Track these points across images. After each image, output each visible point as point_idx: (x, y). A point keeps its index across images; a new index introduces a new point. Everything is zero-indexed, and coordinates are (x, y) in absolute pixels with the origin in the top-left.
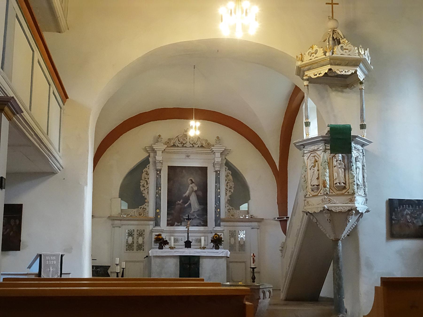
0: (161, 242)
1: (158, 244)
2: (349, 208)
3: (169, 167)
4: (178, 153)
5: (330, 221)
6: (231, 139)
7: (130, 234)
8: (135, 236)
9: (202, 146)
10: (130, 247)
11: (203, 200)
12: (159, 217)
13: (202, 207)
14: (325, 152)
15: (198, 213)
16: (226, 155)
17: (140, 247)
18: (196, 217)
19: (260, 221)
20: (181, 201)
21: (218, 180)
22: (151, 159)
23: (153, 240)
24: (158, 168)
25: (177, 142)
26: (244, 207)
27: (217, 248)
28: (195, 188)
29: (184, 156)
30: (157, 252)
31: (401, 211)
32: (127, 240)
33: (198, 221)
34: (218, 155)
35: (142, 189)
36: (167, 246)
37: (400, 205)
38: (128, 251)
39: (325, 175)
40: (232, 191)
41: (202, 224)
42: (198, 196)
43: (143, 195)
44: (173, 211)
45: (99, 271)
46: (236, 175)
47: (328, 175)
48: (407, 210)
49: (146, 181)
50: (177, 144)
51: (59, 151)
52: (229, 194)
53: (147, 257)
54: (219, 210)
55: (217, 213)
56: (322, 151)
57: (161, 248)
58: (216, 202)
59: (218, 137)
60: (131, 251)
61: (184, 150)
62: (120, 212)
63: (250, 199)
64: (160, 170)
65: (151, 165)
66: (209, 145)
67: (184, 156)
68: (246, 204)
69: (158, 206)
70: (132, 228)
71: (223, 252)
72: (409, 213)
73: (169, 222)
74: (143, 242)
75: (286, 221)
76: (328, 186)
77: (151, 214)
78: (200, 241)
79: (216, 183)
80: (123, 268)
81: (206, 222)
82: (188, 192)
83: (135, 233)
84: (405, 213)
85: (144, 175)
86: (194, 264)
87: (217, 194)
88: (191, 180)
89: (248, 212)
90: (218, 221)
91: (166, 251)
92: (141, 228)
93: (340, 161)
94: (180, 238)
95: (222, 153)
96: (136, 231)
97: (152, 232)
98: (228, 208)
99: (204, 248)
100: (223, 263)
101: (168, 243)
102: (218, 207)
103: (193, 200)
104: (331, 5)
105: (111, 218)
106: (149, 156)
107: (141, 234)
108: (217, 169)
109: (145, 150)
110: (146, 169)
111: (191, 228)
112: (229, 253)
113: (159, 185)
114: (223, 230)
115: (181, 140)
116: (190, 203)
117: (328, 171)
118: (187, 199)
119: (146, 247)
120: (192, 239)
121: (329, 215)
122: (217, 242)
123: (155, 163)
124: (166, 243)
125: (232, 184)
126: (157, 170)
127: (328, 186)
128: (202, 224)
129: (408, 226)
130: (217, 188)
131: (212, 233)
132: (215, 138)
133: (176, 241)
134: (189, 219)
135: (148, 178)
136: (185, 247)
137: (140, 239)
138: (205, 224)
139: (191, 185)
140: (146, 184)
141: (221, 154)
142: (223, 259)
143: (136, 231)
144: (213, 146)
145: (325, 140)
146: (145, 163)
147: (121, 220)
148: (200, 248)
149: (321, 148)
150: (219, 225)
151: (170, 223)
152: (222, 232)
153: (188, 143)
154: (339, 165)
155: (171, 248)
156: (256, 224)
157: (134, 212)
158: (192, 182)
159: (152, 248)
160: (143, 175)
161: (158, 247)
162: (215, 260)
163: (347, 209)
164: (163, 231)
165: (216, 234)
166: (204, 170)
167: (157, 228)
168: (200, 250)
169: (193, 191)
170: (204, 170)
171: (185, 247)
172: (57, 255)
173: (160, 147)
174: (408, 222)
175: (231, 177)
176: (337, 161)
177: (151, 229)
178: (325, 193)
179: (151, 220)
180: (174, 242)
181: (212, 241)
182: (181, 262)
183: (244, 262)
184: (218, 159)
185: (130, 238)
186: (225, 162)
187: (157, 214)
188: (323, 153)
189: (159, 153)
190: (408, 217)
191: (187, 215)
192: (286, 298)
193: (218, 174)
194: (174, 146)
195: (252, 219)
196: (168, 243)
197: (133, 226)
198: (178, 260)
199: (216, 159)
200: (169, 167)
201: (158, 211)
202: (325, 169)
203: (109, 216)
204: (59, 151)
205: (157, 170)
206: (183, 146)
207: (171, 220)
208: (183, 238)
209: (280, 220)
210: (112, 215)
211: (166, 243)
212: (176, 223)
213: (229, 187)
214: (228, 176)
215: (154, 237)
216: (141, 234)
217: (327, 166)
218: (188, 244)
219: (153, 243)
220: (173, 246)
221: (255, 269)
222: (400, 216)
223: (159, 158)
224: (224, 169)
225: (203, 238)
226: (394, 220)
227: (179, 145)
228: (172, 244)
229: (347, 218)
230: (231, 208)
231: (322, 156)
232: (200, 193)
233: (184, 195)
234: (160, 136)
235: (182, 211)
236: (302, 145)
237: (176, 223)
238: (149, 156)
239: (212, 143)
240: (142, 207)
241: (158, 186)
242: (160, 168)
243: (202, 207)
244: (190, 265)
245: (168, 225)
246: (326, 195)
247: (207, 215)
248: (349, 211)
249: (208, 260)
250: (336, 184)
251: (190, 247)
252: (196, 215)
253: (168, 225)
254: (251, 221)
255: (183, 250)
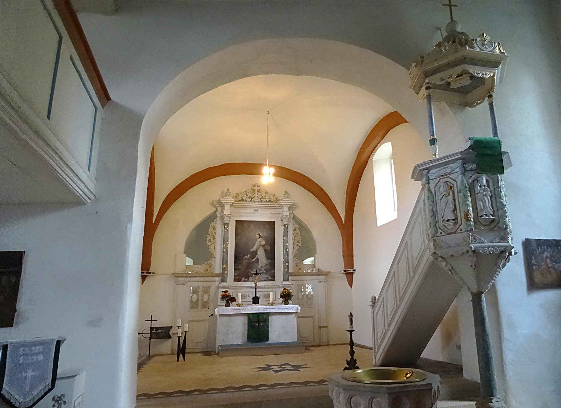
0: (229, 300)
1: (225, 301)
2: (503, 249)
3: (237, 222)
4: (246, 207)
5: (476, 267)
6: (299, 194)
7: (195, 291)
8: (200, 293)
9: (270, 201)
10: (194, 305)
11: (271, 254)
12: (226, 272)
13: (270, 261)
14: (464, 175)
15: (266, 267)
16: (293, 210)
17: (205, 305)
18: (263, 272)
19: (326, 274)
20: (249, 256)
21: (286, 234)
22: (218, 214)
23: (220, 297)
24: (226, 222)
25: (246, 196)
26: (308, 261)
27: (286, 303)
28: (263, 243)
29: (252, 211)
30: (223, 310)
31: (540, 254)
32: (192, 297)
33: (266, 276)
34: (286, 209)
35: (209, 244)
36: (234, 303)
37: (538, 246)
38: (192, 310)
39: (468, 205)
40: (300, 244)
41: (270, 278)
42: (266, 251)
43: (210, 250)
44: (240, 267)
45: (250, 226)
46: (302, 229)
47: (470, 204)
48: (546, 253)
49: (213, 236)
50: (245, 198)
51: (89, 170)
52: (297, 248)
53: (212, 315)
54: (287, 264)
55: (286, 267)
56: (459, 173)
57: (228, 305)
58: (284, 256)
59: (286, 192)
60: (196, 310)
61: (252, 204)
62: (185, 268)
63: (316, 253)
64: (228, 224)
65: (218, 219)
66: (277, 200)
67: (252, 211)
68: (313, 258)
69: (225, 261)
70: (197, 285)
71: (292, 308)
72: (549, 256)
73: (236, 278)
74: (209, 299)
75: (352, 273)
76: (472, 220)
77: (218, 269)
78: (268, 296)
79: (284, 236)
80: (186, 331)
81: (274, 277)
82: (256, 246)
83: (201, 290)
84: (544, 256)
85: (211, 230)
86: (263, 322)
87: (286, 248)
88: (259, 234)
89: (313, 266)
90: (287, 275)
91: (233, 309)
92: (206, 284)
93: (484, 186)
94: (247, 294)
95: (290, 207)
96: (201, 288)
97: (218, 288)
98: (295, 262)
99: (272, 304)
100: (293, 318)
101: (235, 300)
102: (286, 261)
103: (261, 254)
104: (452, 3)
105: (176, 275)
106: (216, 211)
107: (206, 291)
108: (285, 223)
109: (213, 205)
110: (213, 224)
111: (260, 284)
112: (300, 308)
113: (226, 240)
114: (291, 285)
115: (249, 194)
116: (258, 259)
117: (470, 199)
118: (255, 253)
119: (211, 305)
120: (260, 295)
121: (475, 259)
122: (286, 297)
123: (222, 217)
124: (233, 300)
125: (299, 238)
126: (225, 225)
127: (472, 220)
128: (270, 278)
129: (550, 273)
130: (286, 242)
131: (279, 288)
132: (284, 193)
133: (243, 297)
134: (256, 274)
135: (215, 233)
136: (253, 303)
137: (206, 296)
138: (273, 279)
139: (258, 240)
140: (212, 239)
141: (290, 208)
142: (294, 315)
143: (201, 288)
144: (281, 200)
145: (464, 159)
146: (212, 218)
147: (186, 277)
148: (269, 304)
149: (458, 170)
150: (288, 280)
151: (237, 279)
152: (290, 286)
153: (256, 198)
154: (484, 191)
155: (239, 305)
156: (323, 277)
157: (201, 268)
158: (260, 237)
159: (218, 306)
160: (210, 230)
161: (225, 304)
162: (284, 316)
163: (498, 250)
164: (229, 287)
165: (285, 289)
166: (272, 224)
167: (224, 284)
168: (268, 307)
169: (261, 245)
170: (272, 224)
171: (253, 303)
172: (45, 344)
173: (228, 200)
174: (549, 267)
175: (298, 231)
176: (480, 186)
177: (217, 285)
178: (469, 229)
179: (217, 276)
180: (242, 299)
181: (281, 297)
182: (249, 319)
183: (312, 317)
184: (286, 212)
185: (195, 296)
186: (292, 217)
187: (224, 270)
188: (460, 176)
189: (227, 207)
190: (548, 260)
191: (255, 270)
192: (383, 363)
193: (286, 227)
194: (242, 200)
195: (319, 273)
196: (235, 300)
197: (199, 283)
198: (247, 318)
199: (284, 213)
200: (237, 222)
201: (225, 266)
202: (466, 197)
203: (173, 272)
204: (89, 170)
205: (225, 225)
206: (251, 200)
207: (237, 275)
208: (250, 294)
209: (346, 273)
210: (176, 272)
211: (233, 300)
212: (243, 279)
213: (296, 241)
214: (295, 230)
215: (220, 294)
216: (206, 291)
217: (469, 193)
218: (256, 300)
219: (219, 300)
220: (240, 303)
221: (353, 332)
222: (539, 260)
223: (227, 211)
224: (291, 224)
225: (271, 293)
226: (535, 265)
227: (247, 199)
228: (239, 300)
229: (497, 263)
230: (299, 261)
231: (459, 180)
232: (268, 248)
233: (252, 250)
234: (228, 190)
235: (249, 266)
236: (426, 169)
237: (243, 279)
238: (216, 211)
239: (280, 198)
240: (208, 262)
241: (225, 241)
242: (227, 222)
243: (270, 261)
244: (259, 322)
245: (235, 280)
246: (470, 231)
247: (274, 269)
248: (502, 252)
249: (278, 316)
250: (482, 216)
251: (258, 303)
252: (263, 270)
253: (235, 280)
254: (318, 275)
255: (249, 307)
